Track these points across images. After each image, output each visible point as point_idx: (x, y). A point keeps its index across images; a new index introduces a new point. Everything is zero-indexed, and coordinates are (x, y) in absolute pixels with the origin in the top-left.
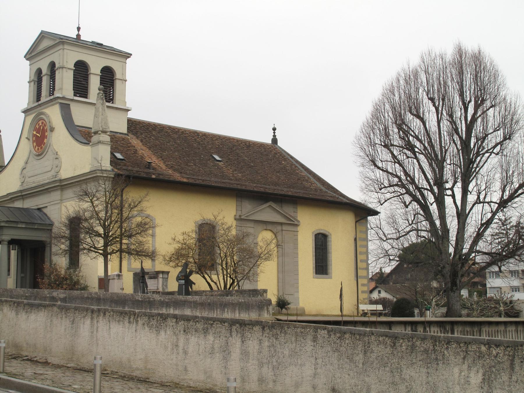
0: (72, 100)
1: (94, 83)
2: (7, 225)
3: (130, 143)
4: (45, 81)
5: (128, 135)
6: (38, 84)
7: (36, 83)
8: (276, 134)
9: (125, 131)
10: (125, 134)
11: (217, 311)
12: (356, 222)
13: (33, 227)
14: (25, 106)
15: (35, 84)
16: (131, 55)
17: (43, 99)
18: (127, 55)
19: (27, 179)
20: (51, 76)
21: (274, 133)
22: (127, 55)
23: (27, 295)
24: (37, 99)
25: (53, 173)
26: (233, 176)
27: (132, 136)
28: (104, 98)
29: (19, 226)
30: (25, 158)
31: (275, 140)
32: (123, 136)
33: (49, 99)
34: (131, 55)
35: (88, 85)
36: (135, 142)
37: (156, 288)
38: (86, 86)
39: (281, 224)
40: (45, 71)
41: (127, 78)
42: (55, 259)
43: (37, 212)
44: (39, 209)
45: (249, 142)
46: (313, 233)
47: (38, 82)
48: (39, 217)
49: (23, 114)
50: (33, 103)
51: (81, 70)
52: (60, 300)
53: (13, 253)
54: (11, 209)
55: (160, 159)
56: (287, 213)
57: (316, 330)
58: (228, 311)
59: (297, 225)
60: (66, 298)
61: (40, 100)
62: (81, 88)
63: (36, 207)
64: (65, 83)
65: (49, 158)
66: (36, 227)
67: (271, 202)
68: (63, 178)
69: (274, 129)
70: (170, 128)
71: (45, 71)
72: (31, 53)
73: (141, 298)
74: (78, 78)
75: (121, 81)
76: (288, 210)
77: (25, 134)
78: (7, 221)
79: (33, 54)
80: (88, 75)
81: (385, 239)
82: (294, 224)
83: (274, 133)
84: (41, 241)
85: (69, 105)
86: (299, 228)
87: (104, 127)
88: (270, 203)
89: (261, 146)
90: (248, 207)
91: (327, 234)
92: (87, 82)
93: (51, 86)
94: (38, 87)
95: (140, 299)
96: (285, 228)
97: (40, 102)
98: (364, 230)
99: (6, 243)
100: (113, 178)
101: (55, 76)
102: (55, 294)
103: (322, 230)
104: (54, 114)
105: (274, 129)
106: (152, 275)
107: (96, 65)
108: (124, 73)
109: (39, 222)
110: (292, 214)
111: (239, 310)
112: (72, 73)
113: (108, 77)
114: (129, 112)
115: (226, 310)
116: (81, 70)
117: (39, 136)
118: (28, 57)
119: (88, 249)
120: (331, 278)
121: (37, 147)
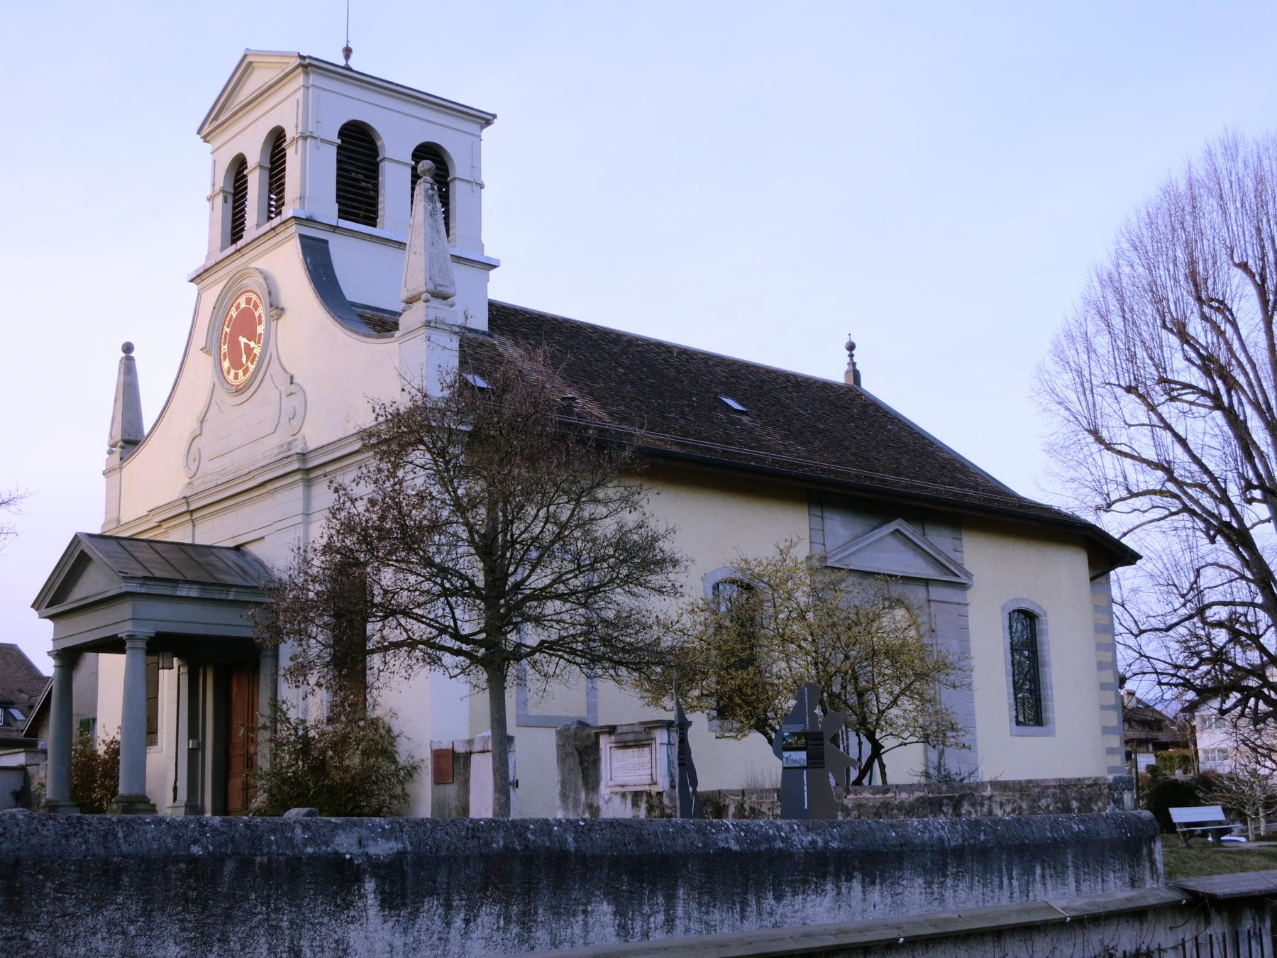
0: (334, 229)
1: (394, 181)
2: (143, 590)
3: (501, 355)
4: (255, 182)
5: (490, 336)
6: (235, 202)
7: (230, 199)
8: (855, 359)
9: (484, 326)
10: (483, 333)
11: (1010, 878)
12: (1092, 579)
13: (223, 596)
14: (199, 261)
15: (225, 201)
16: (495, 116)
17: (250, 231)
18: (486, 120)
19: (207, 466)
20: (271, 170)
21: (851, 356)
22: (486, 120)
23: (196, 849)
24: (233, 234)
25: (281, 437)
26: (780, 449)
27: (503, 339)
28: (436, 198)
29: (178, 593)
30: (199, 409)
31: (856, 375)
32: (480, 338)
33: (267, 226)
34: (495, 116)
35: (377, 191)
36: (510, 350)
37: (647, 779)
38: (372, 193)
39: (926, 582)
40: (254, 158)
41: (485, 178)
42: (287, 692)
43: (231, 554)
44: (237, 548)
45: (795, 376)
46: (1003, 608)
47: (235, 195)
48: (241, 568)
49: (194, 287)
50: (223, 248)
51: (358, 147)
52: (374, 875)
53: (170, 680)
54: (159, 547)
55: (589, 398)
56: (940, 552)
57: (1234, 920)
58: (1043, 876)
59: (963, 586)
60: (401, 855)
61: (241, 237)
62: (358, 193)
63: (231, 544)
64: (312, 179)
65: (269, 391)
66: (231, 597)
67: (899, 521)
68: (311, 447)
69: (851, 347)
70: (595, 329)
71: (254, 158)
72: (216, 118)
73: (738, 840)
74: (349, 171)
75: (469, 185)
76: (941, 540)
77: (200, 340)
78: (145, 578)
79: (221, 119)
80: (377, 165)
81: (1136, 632)
82: (954, 580)
83: (851, 356)
84: (250, 640)
85: (326, 242)
86: (970, 595)
87: (439, 281)
88: (897, 524)
89: (826, 386)
90: (839, 528)
91: (1037, 611)
92: (376, 185)
93: (270, 206)
94: (234, 208)
95: (735, 847)
96: (937, 593)
97: (240, 243)
98: (1105, 604)
99: (142, 645)
100: (470, 434)
101: (283, 184)
102: (345, 843)
103: (1023, 600)
104: (284, 263)
105: (851, 347)
106: (630, 737)
107: (397, 140)
108: (475, 165)
109: (240, 582)
110: (952, 555)
111: (1076, 867)
112: (332, 153)
113: (434, 164)
114: (492, 273)
115: (1038, 871)
116: (358, 147)
117: (235, 333)
118: (206, 130)
119: (429, 643)
120: (1051, 734)
121: (233, 372)
